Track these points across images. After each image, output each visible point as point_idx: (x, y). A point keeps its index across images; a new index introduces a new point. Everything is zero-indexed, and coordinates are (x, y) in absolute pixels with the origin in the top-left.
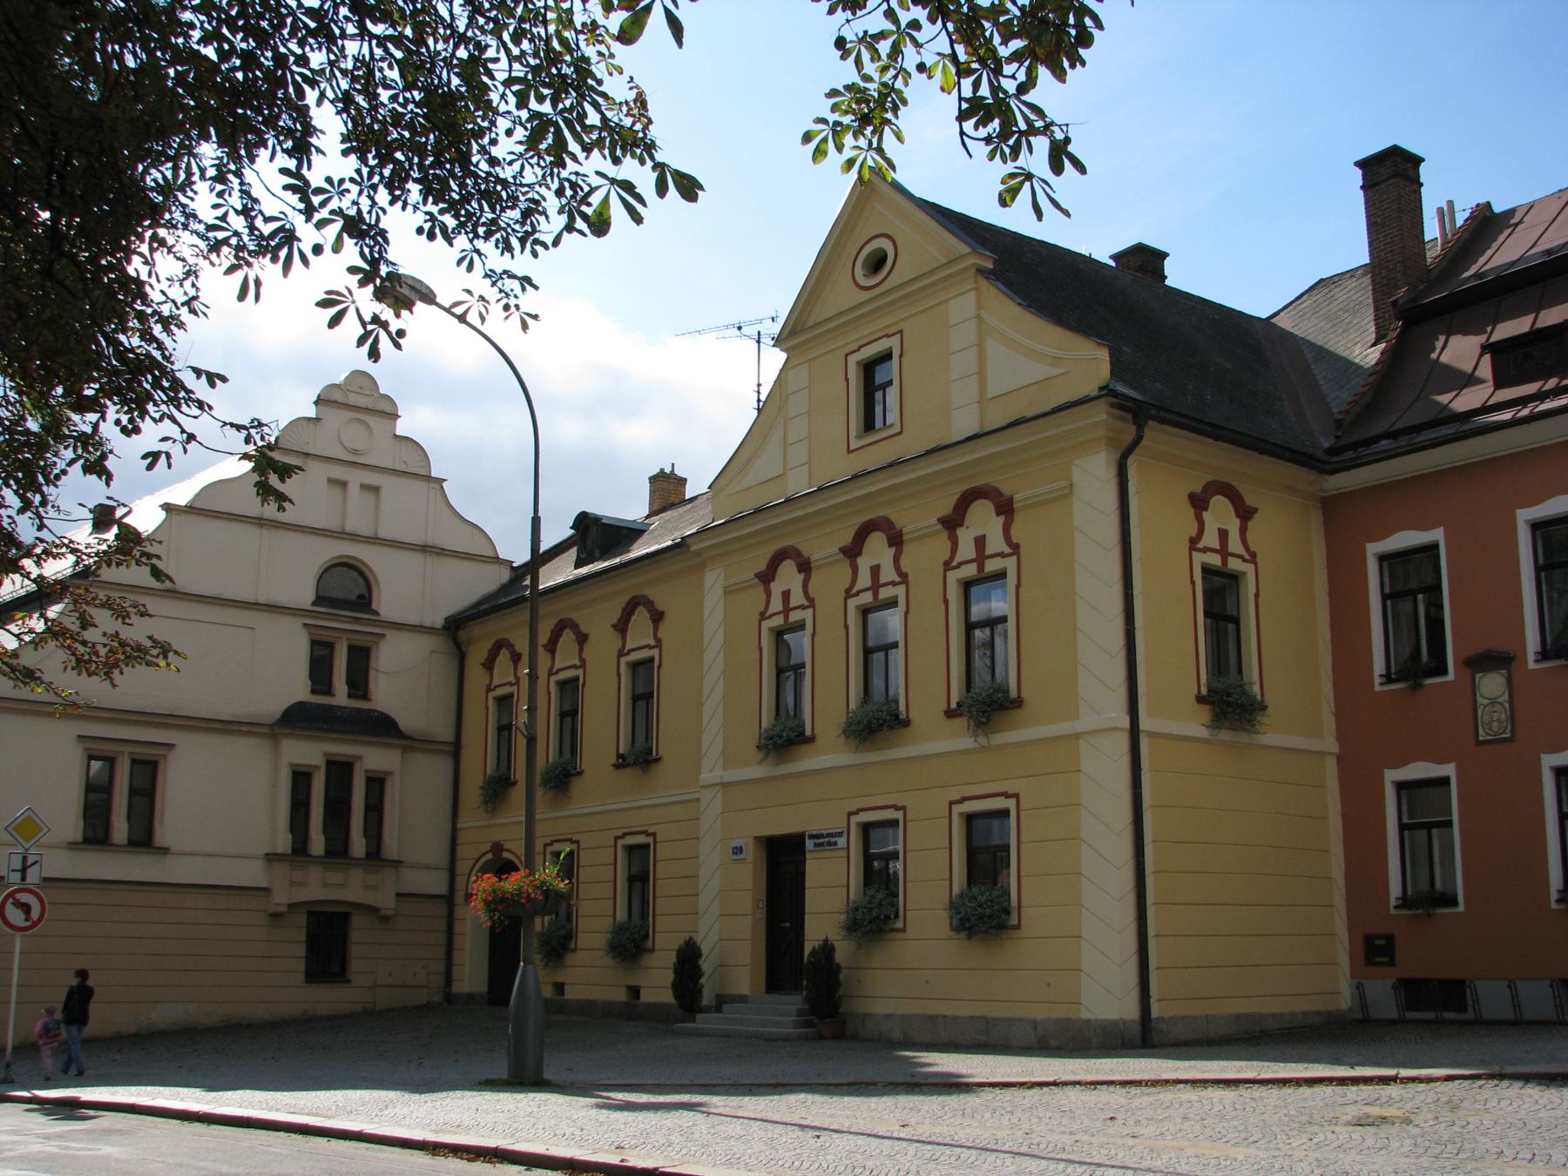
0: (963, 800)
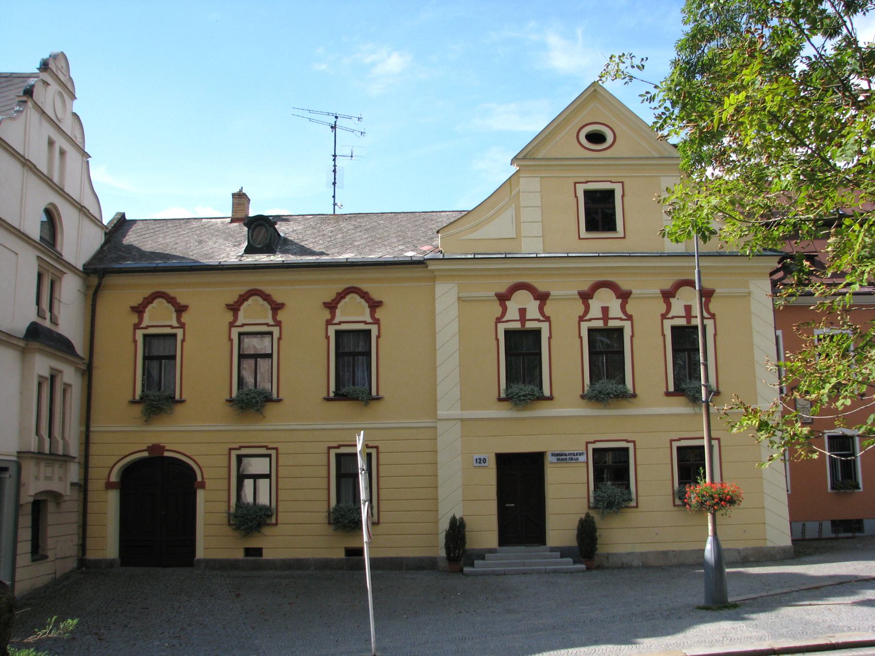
0: (595, 442)
